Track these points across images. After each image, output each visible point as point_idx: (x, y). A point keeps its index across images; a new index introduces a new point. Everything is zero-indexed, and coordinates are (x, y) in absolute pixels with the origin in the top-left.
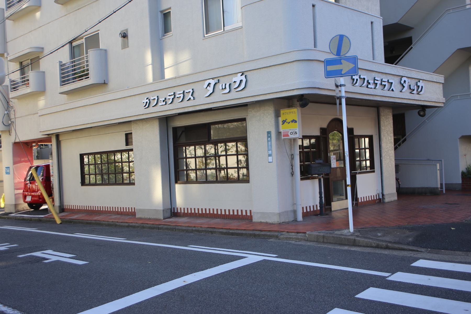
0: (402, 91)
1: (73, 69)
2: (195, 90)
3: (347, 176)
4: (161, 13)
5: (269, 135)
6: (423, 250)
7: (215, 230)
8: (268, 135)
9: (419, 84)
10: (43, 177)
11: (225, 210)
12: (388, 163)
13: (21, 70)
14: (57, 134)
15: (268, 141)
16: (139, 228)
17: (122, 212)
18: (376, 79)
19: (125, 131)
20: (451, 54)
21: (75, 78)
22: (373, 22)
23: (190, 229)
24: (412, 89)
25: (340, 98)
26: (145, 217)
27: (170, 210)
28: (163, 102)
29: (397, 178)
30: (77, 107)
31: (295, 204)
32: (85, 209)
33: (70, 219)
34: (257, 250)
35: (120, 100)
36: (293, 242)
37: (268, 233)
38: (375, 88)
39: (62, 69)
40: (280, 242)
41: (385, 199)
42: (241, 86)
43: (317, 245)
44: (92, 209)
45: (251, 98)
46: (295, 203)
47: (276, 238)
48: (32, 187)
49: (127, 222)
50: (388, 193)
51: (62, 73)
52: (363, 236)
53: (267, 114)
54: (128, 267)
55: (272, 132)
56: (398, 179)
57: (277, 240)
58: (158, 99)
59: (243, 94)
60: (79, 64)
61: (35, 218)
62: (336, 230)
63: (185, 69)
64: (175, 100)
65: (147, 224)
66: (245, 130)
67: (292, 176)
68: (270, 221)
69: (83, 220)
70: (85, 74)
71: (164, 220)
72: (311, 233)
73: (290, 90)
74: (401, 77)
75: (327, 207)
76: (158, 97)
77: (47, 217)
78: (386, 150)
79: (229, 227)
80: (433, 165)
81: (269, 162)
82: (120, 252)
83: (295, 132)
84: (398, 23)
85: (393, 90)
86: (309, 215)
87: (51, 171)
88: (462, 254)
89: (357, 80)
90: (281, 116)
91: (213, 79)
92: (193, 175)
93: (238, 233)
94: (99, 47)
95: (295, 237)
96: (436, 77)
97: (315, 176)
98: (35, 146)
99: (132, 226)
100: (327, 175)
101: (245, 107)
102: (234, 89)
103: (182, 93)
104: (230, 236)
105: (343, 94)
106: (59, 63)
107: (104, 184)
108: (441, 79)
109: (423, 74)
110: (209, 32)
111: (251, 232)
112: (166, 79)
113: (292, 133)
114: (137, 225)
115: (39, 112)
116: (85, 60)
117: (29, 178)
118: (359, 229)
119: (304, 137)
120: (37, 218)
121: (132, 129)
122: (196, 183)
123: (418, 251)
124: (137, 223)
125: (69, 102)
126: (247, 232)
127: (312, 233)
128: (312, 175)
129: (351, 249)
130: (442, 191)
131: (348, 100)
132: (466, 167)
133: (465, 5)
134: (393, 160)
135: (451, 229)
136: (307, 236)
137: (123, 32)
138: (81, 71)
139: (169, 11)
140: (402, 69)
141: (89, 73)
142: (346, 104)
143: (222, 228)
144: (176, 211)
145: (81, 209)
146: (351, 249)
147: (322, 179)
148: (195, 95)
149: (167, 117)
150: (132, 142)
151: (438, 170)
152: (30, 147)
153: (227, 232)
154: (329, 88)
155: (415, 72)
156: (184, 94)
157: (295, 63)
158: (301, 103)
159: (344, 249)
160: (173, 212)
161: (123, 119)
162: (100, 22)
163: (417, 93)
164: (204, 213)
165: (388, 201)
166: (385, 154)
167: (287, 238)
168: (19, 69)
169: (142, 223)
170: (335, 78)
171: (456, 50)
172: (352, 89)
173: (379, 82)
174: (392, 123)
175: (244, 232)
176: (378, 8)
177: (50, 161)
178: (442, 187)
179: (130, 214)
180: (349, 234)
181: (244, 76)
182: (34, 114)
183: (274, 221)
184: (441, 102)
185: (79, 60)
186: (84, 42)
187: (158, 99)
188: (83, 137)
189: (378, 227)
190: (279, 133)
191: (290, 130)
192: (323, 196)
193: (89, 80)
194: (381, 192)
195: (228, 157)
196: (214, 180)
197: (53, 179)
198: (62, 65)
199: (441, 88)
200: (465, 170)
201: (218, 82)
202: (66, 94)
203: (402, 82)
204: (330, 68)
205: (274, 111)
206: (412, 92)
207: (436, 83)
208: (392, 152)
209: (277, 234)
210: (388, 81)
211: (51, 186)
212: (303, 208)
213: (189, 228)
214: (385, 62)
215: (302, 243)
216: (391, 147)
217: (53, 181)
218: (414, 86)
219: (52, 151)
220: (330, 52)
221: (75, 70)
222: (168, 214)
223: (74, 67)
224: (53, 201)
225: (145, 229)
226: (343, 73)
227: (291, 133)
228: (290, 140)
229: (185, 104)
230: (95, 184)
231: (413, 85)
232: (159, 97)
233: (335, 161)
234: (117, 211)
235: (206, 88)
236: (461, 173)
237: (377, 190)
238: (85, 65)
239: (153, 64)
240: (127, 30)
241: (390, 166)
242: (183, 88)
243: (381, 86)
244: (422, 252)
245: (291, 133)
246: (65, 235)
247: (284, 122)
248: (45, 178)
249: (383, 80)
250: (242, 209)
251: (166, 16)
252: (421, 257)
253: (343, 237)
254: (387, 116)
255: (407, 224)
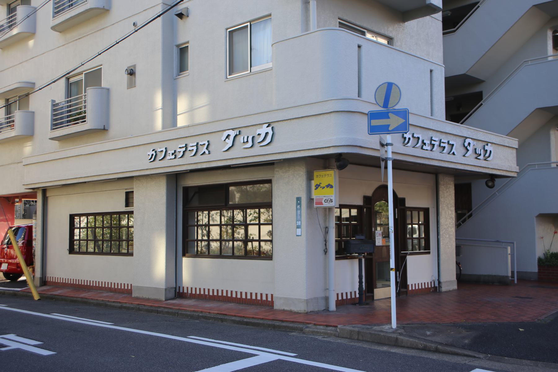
0: (465, 155)
1: (68, 110)
2: (211, 143)
3: (390, 258)
4: (177, 48)
5: (299, 202)
6: (481, 356)
7: (226, 317)
8: (298, 202)
9: (486, 148)
10: (24, 241)
11: (251, 294)
12: (448, 243)
13: (7, 106)
14: (44, 189)
15: (297, 209)
16: (134, 311)
17: (116, 288)
18: (433, 139)
19: (126, 189)
20: (528, 114)
21: (70, 121)
22: (433, 70)
23: (195, 315)
24: (478, 153)
25: (386, 160)
26: (143, 297)
27: (174, 289)
28: (172, 155)
29: (458, 262)
30: (69, 157)
31: (328, 289)
32: (72, 283)
33: (51, 294)
34: (273, 347)
35: (121, 150)
36: (320, 338)
37: (291, 325)
38: (431, 150)
39: (54, 110)
40: (304, 337)
41: (441, 288)
42: (266, 140)
43: (349, 344)
44: (80, 283)
45: (277, 155)
46: (328, 288)
47: (300, 331)
48: (10, 253)
49: (120, 302)
50: (445, 281)
51: (54, 114)
52: (408, 334)
53: (298, 176)
54: (105, 361)
55: (302, 198)
56: (459, 263)
57: (301, 333)
58: (166, 152)
59: (268, 150)
60: (76, 104)
61: (10, 291)
62: (375, 325)
63: (202, 116)
64: (187, 153)
65: (144, 305)
66: (270, 193)
67: (325, 254)
68: (295, 309)
69: (67, 296)
70: (81, 117)
71: (165, 302)
72: (343, 327)
73: (326, 147)
74: (464, 138)
75: (368, 294)
76: (166, 148)
77: (24, 291)
78: (445, 227)
79: (243, 314)
80: (504, 248)
81: (297, 236)
82: (100, 341)
83: (331, 200)
84: (466, 74)
85: (454, 154)
86: (345, 303)
87: (33, 234)
88: (530, 364)
89: (409, 139)
90: (314, 179)
91: (233, 129)
92: (215, 245)
93: (254, 323)
94: (101, 85)
95: (323, 332)
96: (508, 140)
97: (355, 255)
98: (17, 202)
99: (125, 308)
100: (370, 254)
101: (271, 166)
102: (258, 143)
103: (195, 146)
104: (245, 326)
105: (390, 155)
106: (51, 101)
107: (97, 253)
108: (515, 143)
109: (492, 136)
110: (233, 72)
111: (270, 322)
112: (179, 127)
113: (326, 201)
114: (132, 306)
115: (24, 160)
116: (83, 99)
117: (7, 240)
118: (404, 325)
119: (341, 207)
120: (12, 292)
121: (134, 186)
122: (208, 257)
123: (475, 357)
124: (132, 303)
125: (60, 150)
126: (266, 322)
127: (345, 327)
128: (351, 254)
129: (391, 351)
130: (514, 280)
131: (395, 162)
132: (544, 252)
133: (547, 56)
134: (454, 239)
135: (519, 330)
136: (339, 331)
137: (130, 69)
138: (78, 112)
139: (186, 45)
140: (466, 129)
141: (85, 116)
142: (393, 168)
143: (235, 316)
144: (181, 291)
145: (67, 282)
146: (391, 351)
147: (363, 260)
148: (210, 148)
149: (176, 174)
150: (133, 202)
151: (509, 254)
152: (12, 203)
153: (241, 320)
154: (373, 148)
155: (482, 132)
156: (197, 147)
157: (333, 115)
158: (338, 164)
159: (383, 350)
160: (177, 292)
161: (124, 174)
162: (100, 54)
163: (485, 158)
164: (215, 295)
165: (445, 290)
166: (443, 232)
167: (313, 333)
168: (4, 105)
169: (138, 304)
170: (380, 135)
171: (534, 110)
172: (401, 149)
173: (437, 143)
174: (454, 194)
175: (261, 322)
176: (441, 54)
177: (34, 221)
178: (513, 276)
179: (125, 292)
180: (391, 331)
181: (270, 128)
182: (18, 163)
183: (299, 309)
184: (514, 172)
185: (77, 99)
186: (83, 78)
187: (166, 152)
188: (75, 194)
189: (428, 324)
190: (310, 200)
191: (325, 196)
192: (364, 280)
193: (85, 124)
194: (437, 278)
195: (262, 226)
196: (239, 254)
197: (35, 244)
198: (54, 105)
199: (515, 155)
200: (542, 256)
201: (239, 134)
202: (58, 141)
203: (466, 144)
204: (375, 122)
205: (305, 172)
206: (478, 158)
207: (507, 148)
208: (452, 230)
209: (301, 326)
210: (448, 142)
211: (33, 252)
212: (338, 294)
213: (195, 314)
214: (446, 119)
215: (331, 340)
216: (452, 224)
217: (35, 246)
218: (481, 150)
219: (36, 209)
220: (375, 102)
221: (70, 111)
222: (172, 294)
223: (70, 107)
224: (34, 271)
225: (141, 312)
226: (390, 129)
227: (326, 201)
228: (325, 209)
229: (199, 158)
230: (87, 253)
231: (479, 148)
232: (168, 149)
233: (381, 237)
234: (110, 287)
235: (225, 140)
236: (538, 259)
237: (433, 276)
238: (82, 106)
239: (163, 108)
240: (135, 66)
241: (450, 246)
242: (197, 139)
243: (439, 147)
244: (480, 358)
245: (326, 201)
246: (38, 316)
247: (317, 186)
248: (26, 241)
249: (442, 141)
250: (261, 293)
251: (183, 51)
252: (477, 365)
253: (382, 334)
254: (448, 186)
255: (465, 321)
